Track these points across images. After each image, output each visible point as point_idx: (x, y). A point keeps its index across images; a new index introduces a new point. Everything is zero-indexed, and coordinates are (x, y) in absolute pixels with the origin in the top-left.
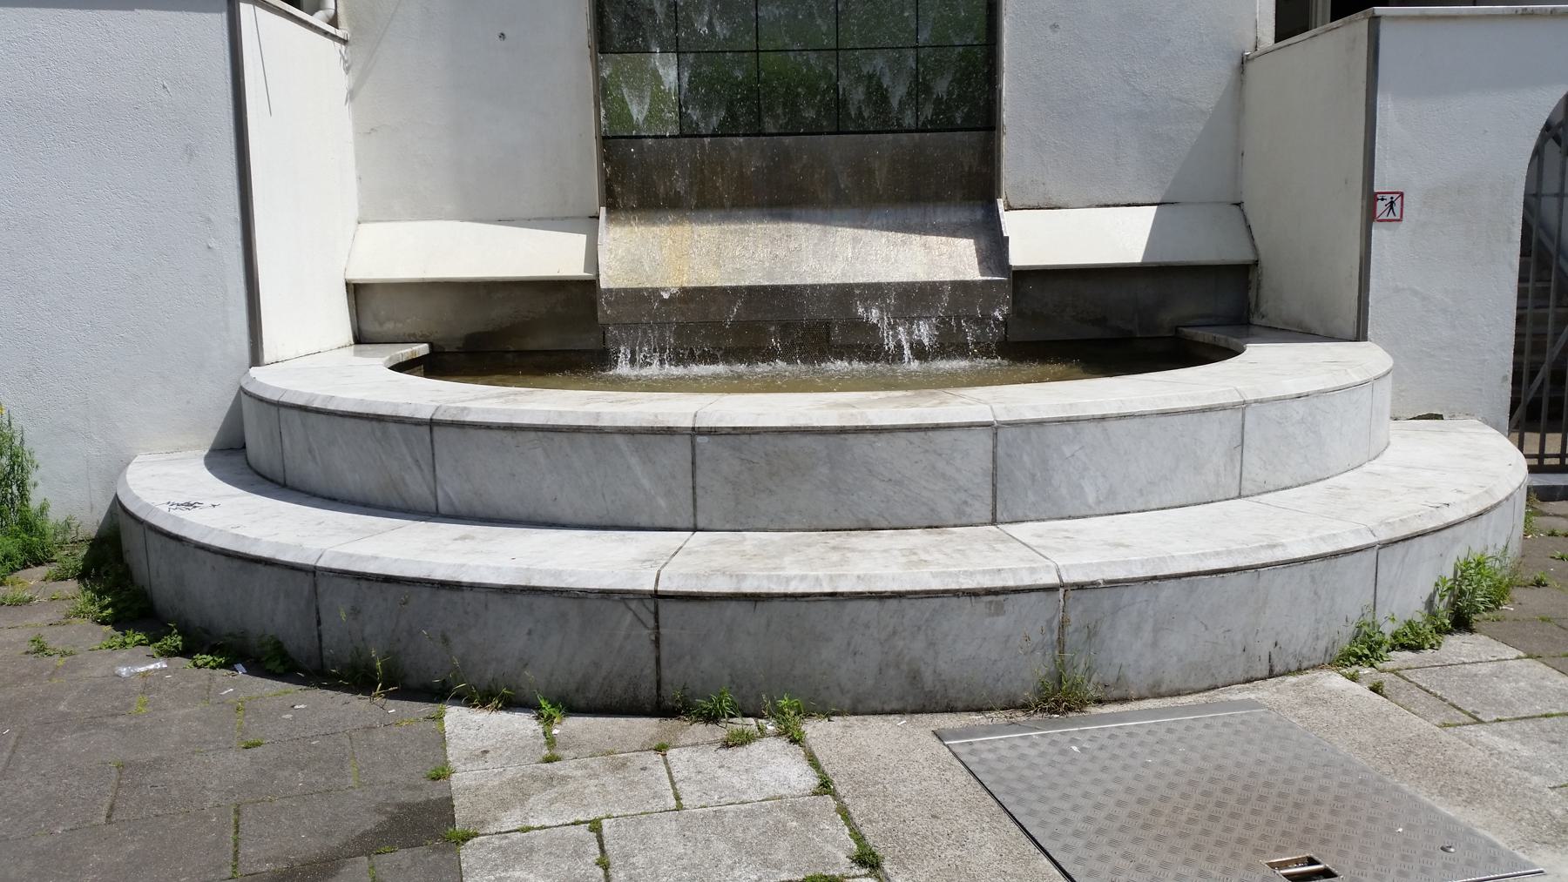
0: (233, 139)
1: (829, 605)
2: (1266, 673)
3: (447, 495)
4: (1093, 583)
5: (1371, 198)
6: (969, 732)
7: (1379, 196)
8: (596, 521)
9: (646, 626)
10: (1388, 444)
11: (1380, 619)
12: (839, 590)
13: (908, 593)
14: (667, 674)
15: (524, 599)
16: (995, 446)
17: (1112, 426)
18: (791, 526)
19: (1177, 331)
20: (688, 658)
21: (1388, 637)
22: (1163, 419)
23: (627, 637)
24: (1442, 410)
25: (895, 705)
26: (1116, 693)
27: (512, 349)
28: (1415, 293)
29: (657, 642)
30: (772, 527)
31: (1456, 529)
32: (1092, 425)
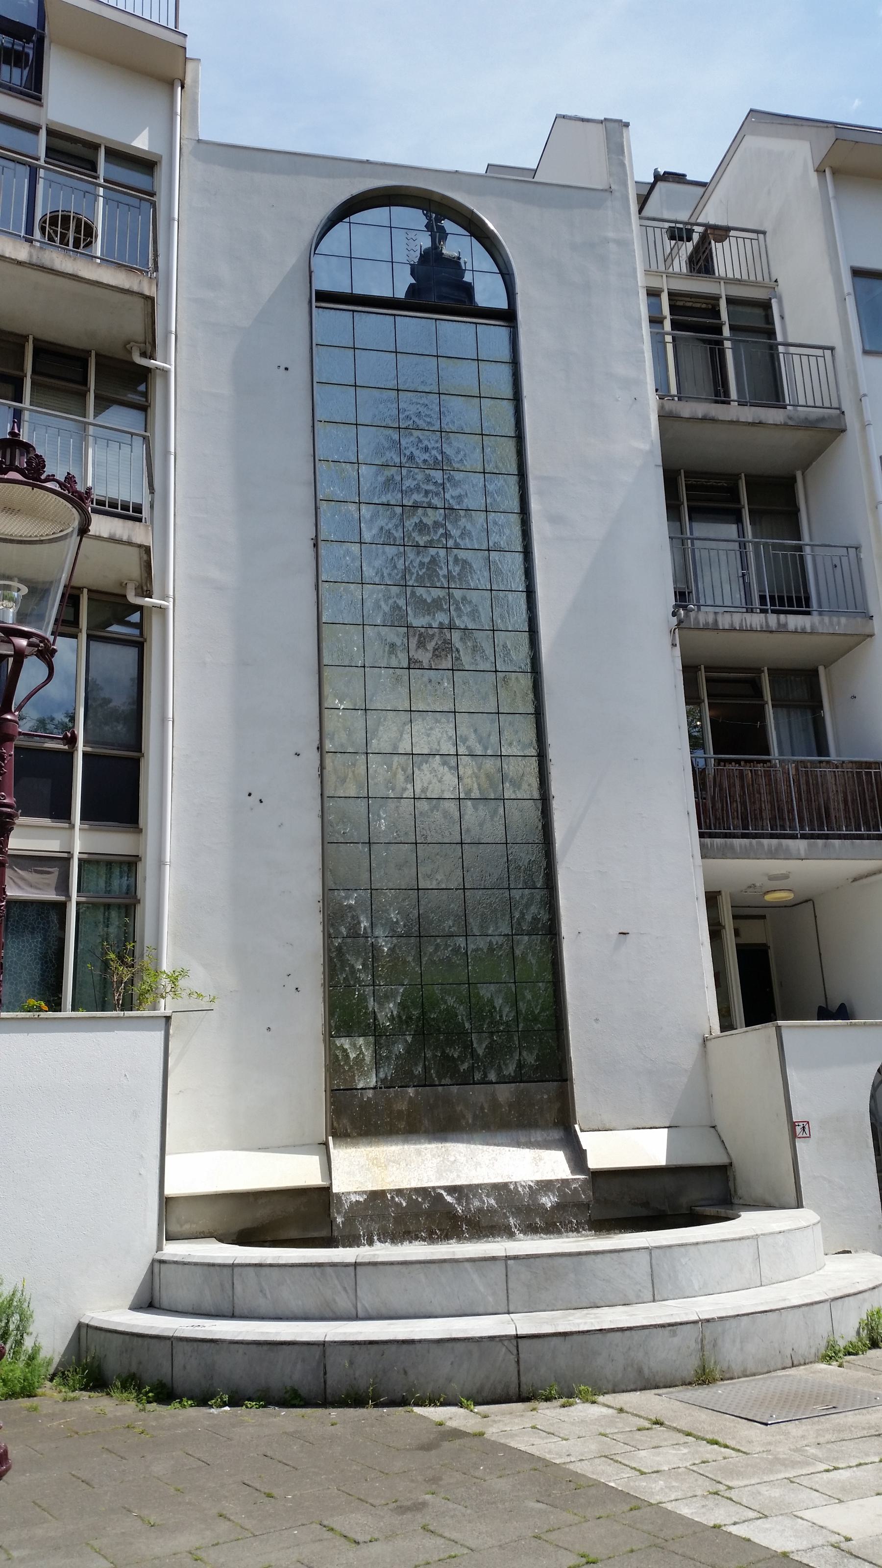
1: (599, 1336)
3: (363, 1306)
4: (713, 1319)
5: (793, 1125)
6: (672, 1393)
7: (796, 1124)
8: (454, 1312)
10: (825, 1265)
11: (837, 1338)
12: (604, 1328)
13: (634, 1327)
14: (523, 1379)
15: (449, 1345)
16: (651, 1260)
17: (701, 1247)
20: (534, 1369)
25: (632, 1387)
26: (728, 1376)
29: (518, 1362)
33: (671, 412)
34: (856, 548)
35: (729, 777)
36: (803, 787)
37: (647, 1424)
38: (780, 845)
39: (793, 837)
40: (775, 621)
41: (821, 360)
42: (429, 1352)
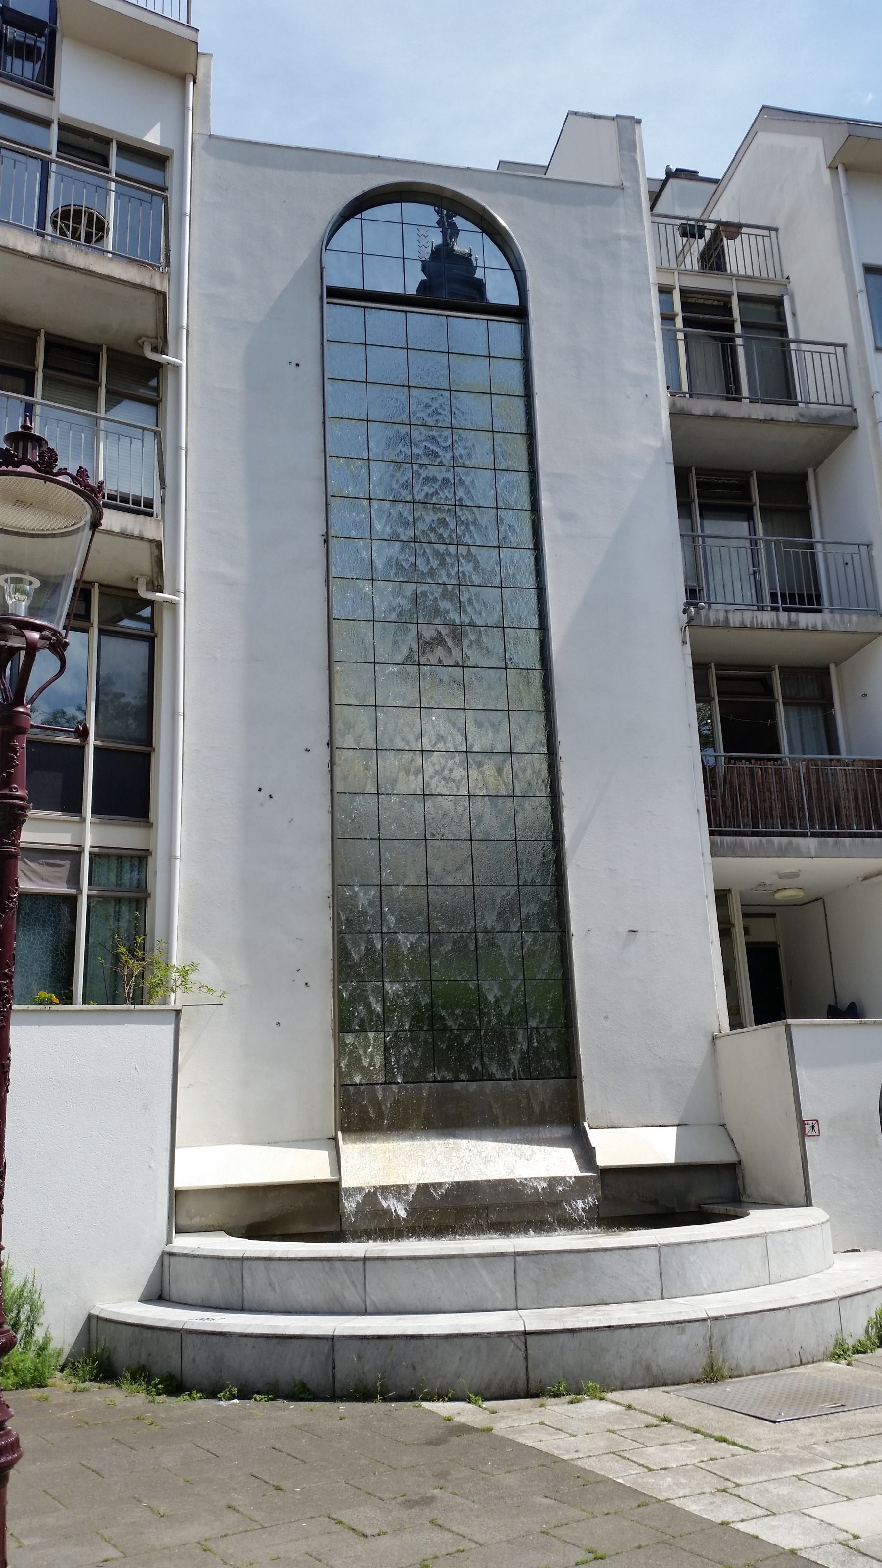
0: (170, 1099)
1: (608, 1332)
2: (799, 1363)
4: (722, 1316)
5: (802, 1124)
6: (680, 1390)
7: (806, 1122)
8: (462, 1308)
9: (520, 1350)
13: (643, 1324)
14: (531, 1375)
15: (457, 1341)
16: (659, 1257)
17: (710, 1245)
18: (566, 1304)
19: (700, 1208)
21: (850, 1347)
22: (732, 1241)
23: (511, 1357)
24: (859, 1246)
25: (641, 1384)
26: (736, 1373)
27: (278, 1233)
28: (833, 1177)
29: (526, 1358)
30: (556, 1305)
31: (873, 1292)
32: (702, 1245)
33: (682, 409)
34: (868, 546)
35: (739, 775)
36: (814, 786)
37: (655, 1421)
38: (791, 843)
39: (804, 835)
40: (787, 619)
41: (833, 357)
42: (437, 1346)
